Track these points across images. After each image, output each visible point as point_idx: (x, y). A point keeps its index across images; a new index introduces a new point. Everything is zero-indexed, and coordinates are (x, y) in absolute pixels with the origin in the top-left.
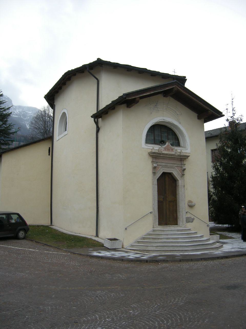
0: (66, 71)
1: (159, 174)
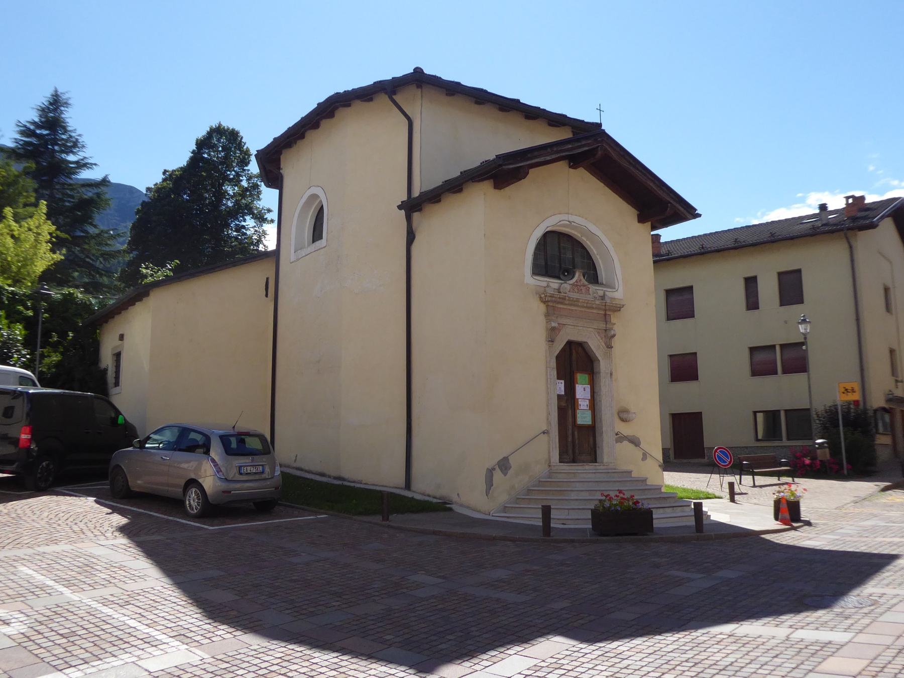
0: (331, 93)
1: (559, 346)
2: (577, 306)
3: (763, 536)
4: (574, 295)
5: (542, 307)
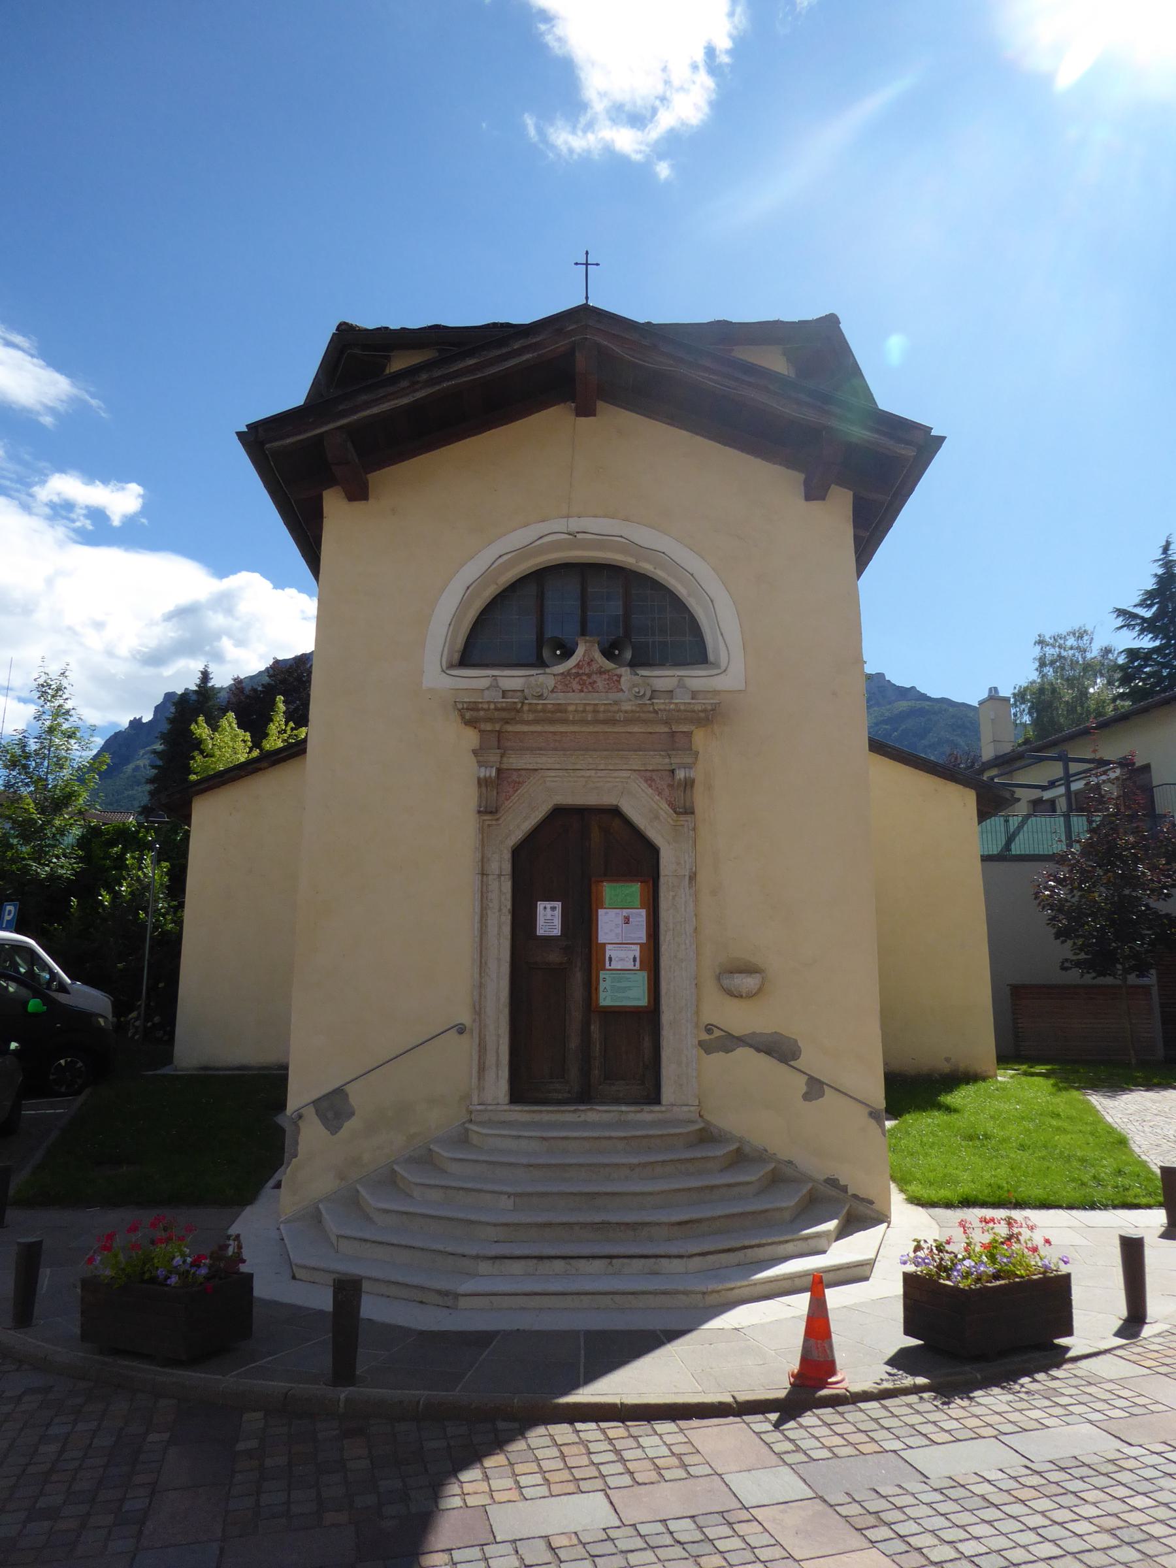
1: (521, 820)
2: (564, 721)
3: (921, 1381)
4: (574, 699)
5: (471, 738)
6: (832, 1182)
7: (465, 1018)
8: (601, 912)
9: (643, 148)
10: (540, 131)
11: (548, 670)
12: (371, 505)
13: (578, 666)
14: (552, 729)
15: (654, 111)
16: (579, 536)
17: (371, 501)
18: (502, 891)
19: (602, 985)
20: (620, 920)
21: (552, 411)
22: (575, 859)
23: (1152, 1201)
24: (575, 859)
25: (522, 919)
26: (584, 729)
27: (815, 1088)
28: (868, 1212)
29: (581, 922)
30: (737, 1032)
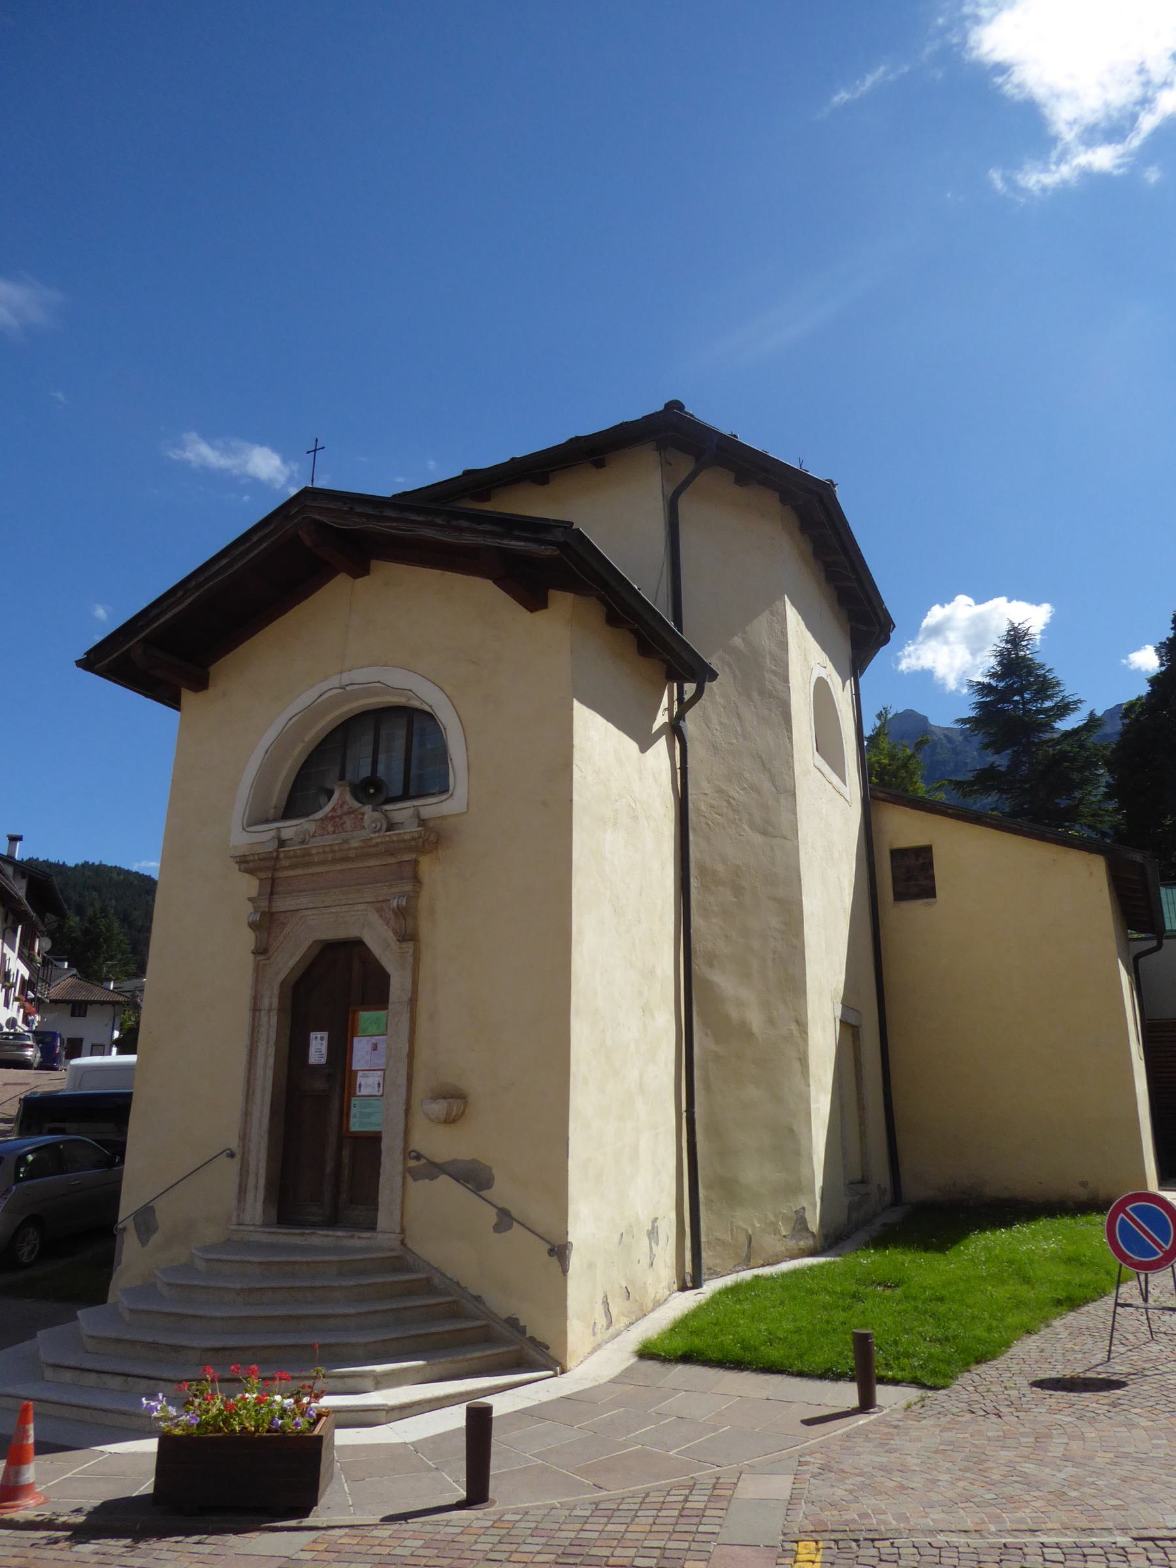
1: (289, 957)
6: (513, 1322)
7: (234, 1144)
8: (356, 1040)
9: (1126, 160)
10: (1008, 180)
11: (311, 817)
12: (211, 691)
13: (334, 810)
14: (310, 871)
15: (1134, 118)
16: (348, 688)
17: (211, 688)
18: (270, 1024)
19: (353, 1111)
20: (369, 1048)
21: (333, 582)
22: (333, 989)
23: (900, 1375)
24: (333, 989)
25: (295, 1047)
26: (332, 868)
27: (505, 1220)
28: (538, 1357)
29: (340, 1051)
30: (438, 1159)
